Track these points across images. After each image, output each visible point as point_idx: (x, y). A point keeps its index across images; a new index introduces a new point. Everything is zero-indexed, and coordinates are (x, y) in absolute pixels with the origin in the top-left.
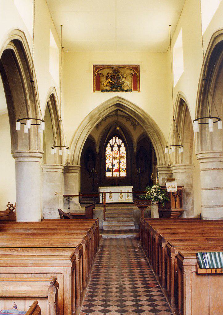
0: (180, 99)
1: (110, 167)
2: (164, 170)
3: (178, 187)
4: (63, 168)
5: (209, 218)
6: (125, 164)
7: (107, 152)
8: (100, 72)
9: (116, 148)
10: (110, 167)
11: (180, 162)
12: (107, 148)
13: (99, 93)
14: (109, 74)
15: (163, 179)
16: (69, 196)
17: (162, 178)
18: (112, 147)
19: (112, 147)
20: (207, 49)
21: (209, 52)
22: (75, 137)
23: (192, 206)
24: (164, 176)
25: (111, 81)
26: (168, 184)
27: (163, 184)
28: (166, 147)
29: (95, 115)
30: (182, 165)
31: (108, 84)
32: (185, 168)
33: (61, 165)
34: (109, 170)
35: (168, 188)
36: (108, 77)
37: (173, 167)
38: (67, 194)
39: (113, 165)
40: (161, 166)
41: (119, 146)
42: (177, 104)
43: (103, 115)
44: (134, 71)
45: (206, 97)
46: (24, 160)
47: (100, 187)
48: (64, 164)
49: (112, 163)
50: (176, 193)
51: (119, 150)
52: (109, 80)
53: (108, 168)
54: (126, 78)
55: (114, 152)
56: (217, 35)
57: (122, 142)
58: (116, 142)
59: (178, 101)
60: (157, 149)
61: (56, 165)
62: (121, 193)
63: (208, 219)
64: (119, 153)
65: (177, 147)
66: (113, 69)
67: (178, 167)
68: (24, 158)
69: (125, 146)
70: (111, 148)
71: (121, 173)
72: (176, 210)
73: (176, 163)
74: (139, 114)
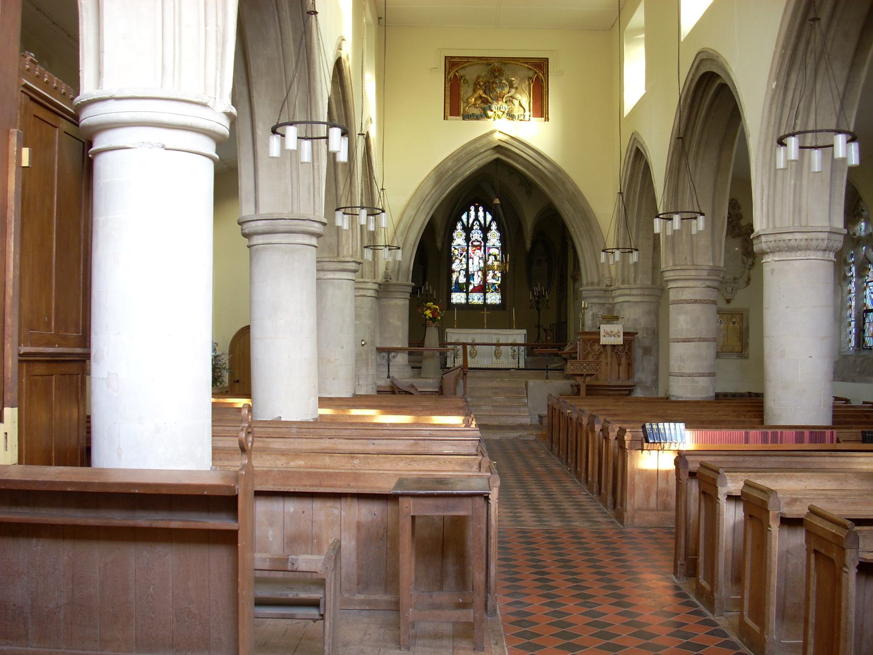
0: (635, 147)
1: (462, 280)
2: (595, 297)
3: (625, 334)
4: (376, 287)
5: (681, 397)
6: (499, 275)
7: (455, 243)
8: (461, 73)
9: (476, 235)
10: (462, 280)
11: (632, 281)
12: (455, 235)
13: (457, 123)
14: (481, 79)
15: (594, 316)
16: (389, 351)
17: (591, 313)
18: (468, 230)
19: (468, 230)
20: (689, 73)
21: (692, 80)
22: (404, 220)
23: (655, 377)
24: (595, 310)
25: (484, 95)
26: (605, 328)
27: (592, 327)
28: (603, 251)
29: (447, 171)
30: (635, 286)
31: (479, 102)
32: (642, 293)
33: (375, 281)
34: (460, 288)
35: (604, 336)
36: (479, 87)
37: (617, 291)
38: (384, 346)
39: (469, 276)
40: (591, 288)
41: (485, 229)
42: (630, 157)
43: (465, 171)
44: (536, 73)
45: (684, 161)
46: (327, 277)
47: (447, 330)
48: (380, 279)
49: (467, 270)
50: (622, 348)
51: (485, 239)
52: (481, 92)
53: (457, 282)
54: (517, 88)
55: (472, 243)
56: (704, 50)
57: (493, 220)
58: (476, 218)
59: (631, 151)
60: (582, 250)
61: (364, 282)
62: (498, 345)
63: (680, 400)
64: (485, 246)
65: (627, 251)
66: (489, 67)
67: (627, 292)
68: (326, 273)
69: (498, 229)
70: (464, 234)
71: (488, 295)
72: (620, 383)
73: (623, 282)
74: (546, 171)
